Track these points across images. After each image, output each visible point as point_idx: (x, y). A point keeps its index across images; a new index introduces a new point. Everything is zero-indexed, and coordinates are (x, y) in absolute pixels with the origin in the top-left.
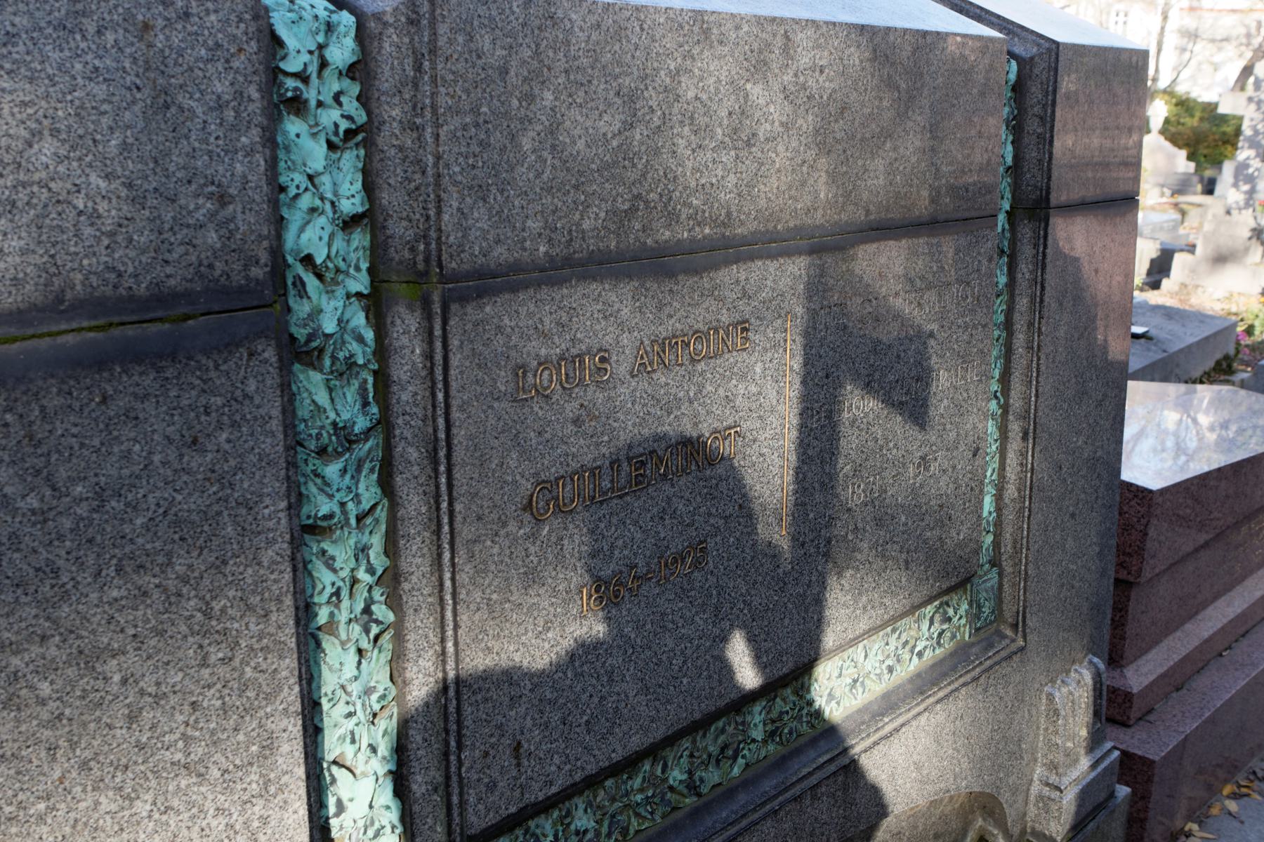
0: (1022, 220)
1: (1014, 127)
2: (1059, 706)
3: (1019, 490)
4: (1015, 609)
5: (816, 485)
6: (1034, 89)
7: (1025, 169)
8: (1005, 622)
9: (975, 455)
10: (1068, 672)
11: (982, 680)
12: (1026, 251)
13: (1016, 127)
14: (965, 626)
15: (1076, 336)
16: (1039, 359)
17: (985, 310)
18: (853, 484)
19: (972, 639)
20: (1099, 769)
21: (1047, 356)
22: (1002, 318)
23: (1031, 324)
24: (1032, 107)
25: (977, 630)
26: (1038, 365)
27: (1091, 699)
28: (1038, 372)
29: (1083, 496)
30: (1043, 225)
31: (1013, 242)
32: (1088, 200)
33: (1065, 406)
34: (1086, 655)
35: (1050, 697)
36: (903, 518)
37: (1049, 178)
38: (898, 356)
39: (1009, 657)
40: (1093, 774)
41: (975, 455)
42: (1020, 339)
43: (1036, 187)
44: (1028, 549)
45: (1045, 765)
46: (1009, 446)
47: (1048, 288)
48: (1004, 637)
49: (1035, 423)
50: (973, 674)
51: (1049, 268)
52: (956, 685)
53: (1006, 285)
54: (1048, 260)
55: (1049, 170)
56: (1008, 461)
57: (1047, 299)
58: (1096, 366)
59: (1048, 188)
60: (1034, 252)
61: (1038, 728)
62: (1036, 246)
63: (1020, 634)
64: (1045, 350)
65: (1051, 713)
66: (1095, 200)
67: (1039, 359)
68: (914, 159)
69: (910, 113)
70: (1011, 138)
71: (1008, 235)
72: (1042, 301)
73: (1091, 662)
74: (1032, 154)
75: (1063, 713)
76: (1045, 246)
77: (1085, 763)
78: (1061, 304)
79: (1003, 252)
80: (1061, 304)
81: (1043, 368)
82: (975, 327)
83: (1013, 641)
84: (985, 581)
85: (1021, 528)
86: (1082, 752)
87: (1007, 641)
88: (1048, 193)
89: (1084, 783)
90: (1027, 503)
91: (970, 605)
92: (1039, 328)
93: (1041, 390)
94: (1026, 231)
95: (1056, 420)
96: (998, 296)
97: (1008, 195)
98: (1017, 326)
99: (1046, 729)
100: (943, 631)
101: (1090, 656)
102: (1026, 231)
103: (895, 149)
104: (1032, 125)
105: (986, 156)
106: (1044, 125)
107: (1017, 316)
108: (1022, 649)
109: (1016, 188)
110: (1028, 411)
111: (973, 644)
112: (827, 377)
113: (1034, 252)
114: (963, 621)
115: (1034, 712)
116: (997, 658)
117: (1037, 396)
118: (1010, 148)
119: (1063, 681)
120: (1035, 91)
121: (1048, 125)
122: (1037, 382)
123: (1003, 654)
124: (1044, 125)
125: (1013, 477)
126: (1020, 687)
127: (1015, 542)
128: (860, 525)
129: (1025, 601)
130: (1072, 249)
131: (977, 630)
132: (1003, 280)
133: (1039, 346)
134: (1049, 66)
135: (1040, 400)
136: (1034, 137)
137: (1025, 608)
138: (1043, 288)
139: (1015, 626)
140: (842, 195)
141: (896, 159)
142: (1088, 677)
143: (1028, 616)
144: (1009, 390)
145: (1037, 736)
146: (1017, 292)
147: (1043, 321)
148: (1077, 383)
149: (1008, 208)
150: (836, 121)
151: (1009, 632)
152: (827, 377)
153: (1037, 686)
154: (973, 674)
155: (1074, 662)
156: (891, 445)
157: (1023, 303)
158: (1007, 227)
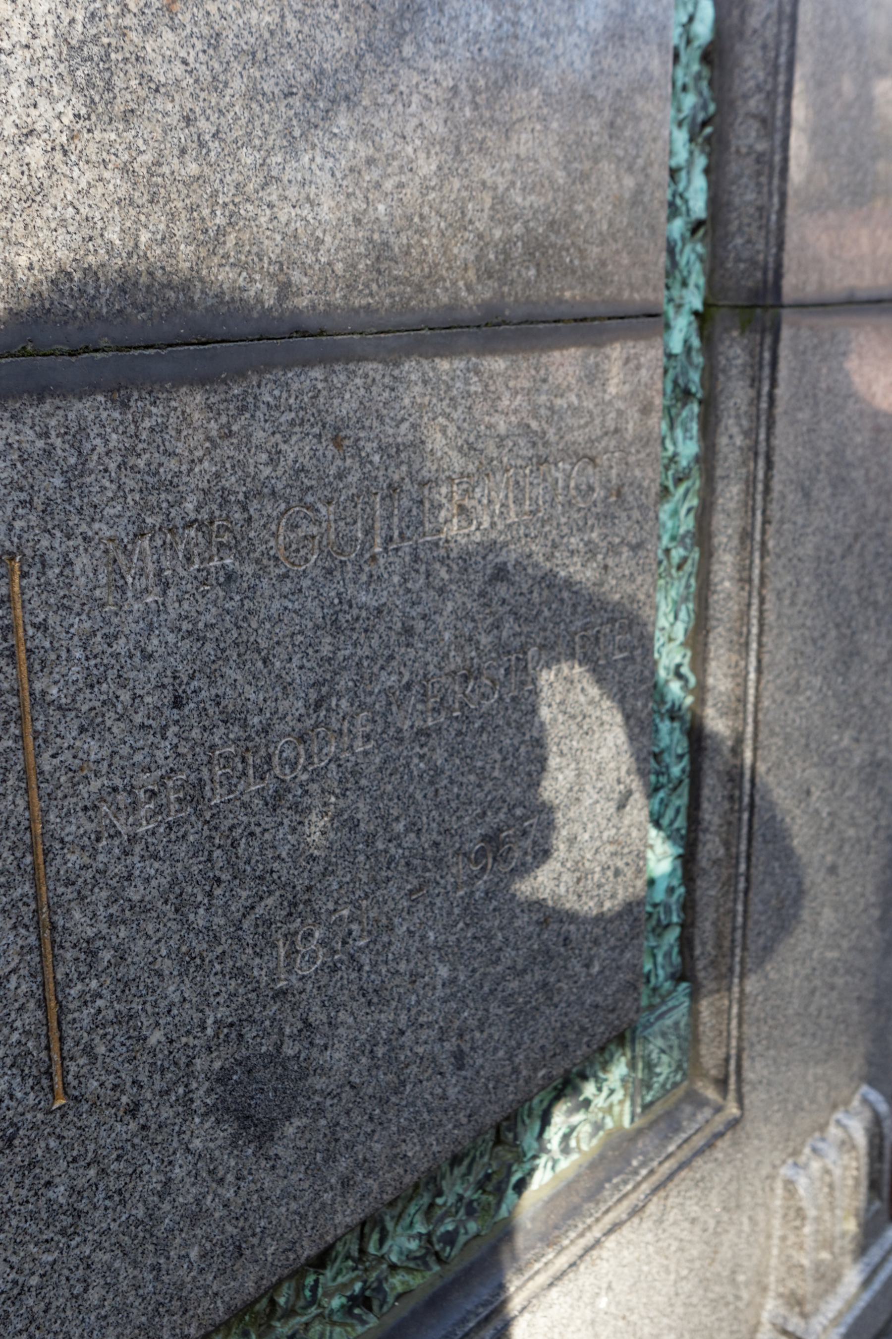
0: (727, 330)
1: (708, 140)
2: (804, 1204)
3: (727, 844)
4: (721, 1053)
5: (166, 966)
6: (748, 60)
7: (733, 227)
8: (705, 1075)
9: (621, 806)
10: (822, 1128)
11: (652, 1208)
12: (737, 395)
13: (711, 133)
14: (621, 1102)
15: (838, 551)
16: (762, 601)
17: (636, 514)
18: (290, 936)
19: (639, 1122)
20: (877, 1285)
21: (779, 595)
22: (687, 524)
23: (746, 535)
24: (746, 97)
25: (646, 1107)
26: (761, 612)
27: (864, 1170)
28: (761, 625)
29: (851, 832)
30: (768, 340)
31: (710, 374)
32: (862, 295)
33: (817, 682)
34: (857, 1088)
35: (789, 1184)
36: (444, 972)
37: (781, 246)
38: (408, 631)
39: (710, 1145)
40: (867, 1297)
41: (621, 806)
42: (725, 566)
43: (753, 262)
44: (745, 948)
45: (780, 1295)
46: (706, 765)
47: (779, 464)
48: (700, 1102)
49: (756, 722)
50: (633, 1200)
51: (781, 426)
52: (597, 1232)
53: (697, 459)
54: (779, 410)
55: (781, 229)
56: (706, 792)
57: (777, 486)
58: (875, 604)
59: (779, 265)
60: (752, 393)
61: (769, 1237)
62: (755, 382)
63: (732, 1095)
64: (775, 583)
65: (792, 1214)
66: (875, 295)
67: (762, 601)
68: (427, 167)
69: (408, 50)
70: (701, 162)
71: (698, 359)
72: (767, 490)
73: (865, 1101)
74: (745, 196)
75: (812, 1213)
76: (774, 383)
77: (852, 1277)
78: (807, 495)
79: (686, 395)
80: (807, 495)
81: (770, 617)
82: (613, 550)
83: (718, 1109)
84: (661, 1016)
85: (733, 913)
86: (848, 1259)
87: (707, 1112)
88: (779, 275)
89: (849, 1319)
90: (743, 867)
91: (632, 1065)
92: (763, 543)
93: (766, 658)
94: (735, 351)
95: (798, 710)
96: (678, 481)
97: (697, 278)
98: (720, 539)
99: (784, 1238)
100: (573, 1129)
101: (865, 1089)
102: (735, 351)
103: (366, 134)
104: (746, 136)
105: (629, 182)
106: (770, 135)
107: (719, 520)
108: (734, 1124)
109: (714, 266)
110: (742, 700)
111: (640, 1132)
112: (177, 703)
113: (752, 393)
114: (619, 1095)
115: (761, 1216)
116: (682, 1156)
117: (759, 670)
118: (699, 182)
119: (815, 1150)
120: (751, 67)
121: (778, 137)
122: (760, 645)
123: (699, 1141)
124: (770, 135)
125: (716, 820)
126: (732, 1188)
127: (719, 936)
128: (318, 1016)
129: (740, 1039)
130: (690, 324)
131: (646, 1107)
132: (688, 449)
133: (762, 576)
134: (780, 12)
135: (767, 677)
136: (750, 161)
137: (740, 1050)
138: (769, 465)
139: (722, 1084)
140: (189, 239)
141: (370, 162)
142: (858, 1130)
143: (746, 1064)
144: (705, 660)
145: (766, 1251)
146: (719, 472)
147: (771, 529)
148: (841, 637)
149: (698, 305)
150: (148, 29)
151: (711, 1093)
152: (177, 703)
153: (765, 1171)
154: (633, 1200)
155: (835, 1107)
156: (400, 827)
157: (730, 494)
158: (696, 342)
